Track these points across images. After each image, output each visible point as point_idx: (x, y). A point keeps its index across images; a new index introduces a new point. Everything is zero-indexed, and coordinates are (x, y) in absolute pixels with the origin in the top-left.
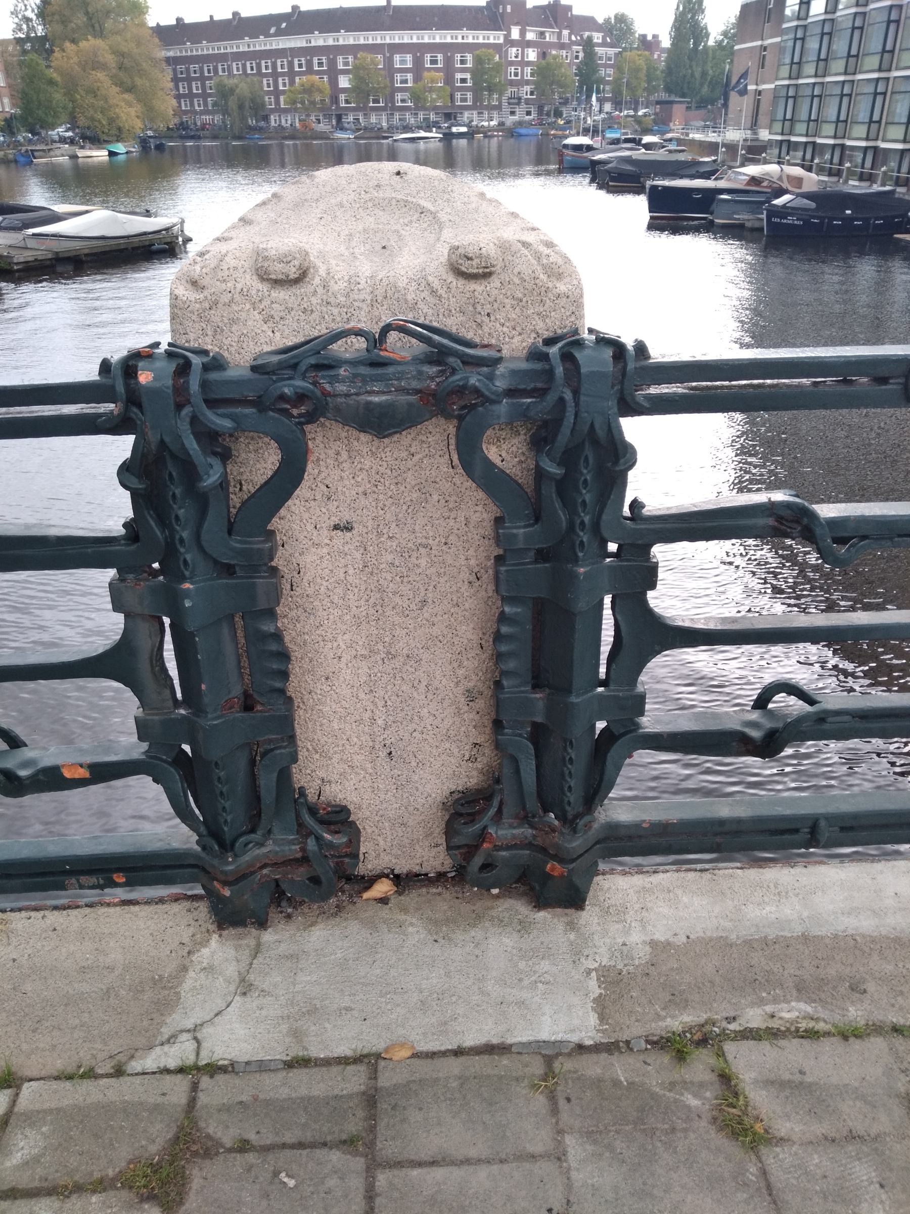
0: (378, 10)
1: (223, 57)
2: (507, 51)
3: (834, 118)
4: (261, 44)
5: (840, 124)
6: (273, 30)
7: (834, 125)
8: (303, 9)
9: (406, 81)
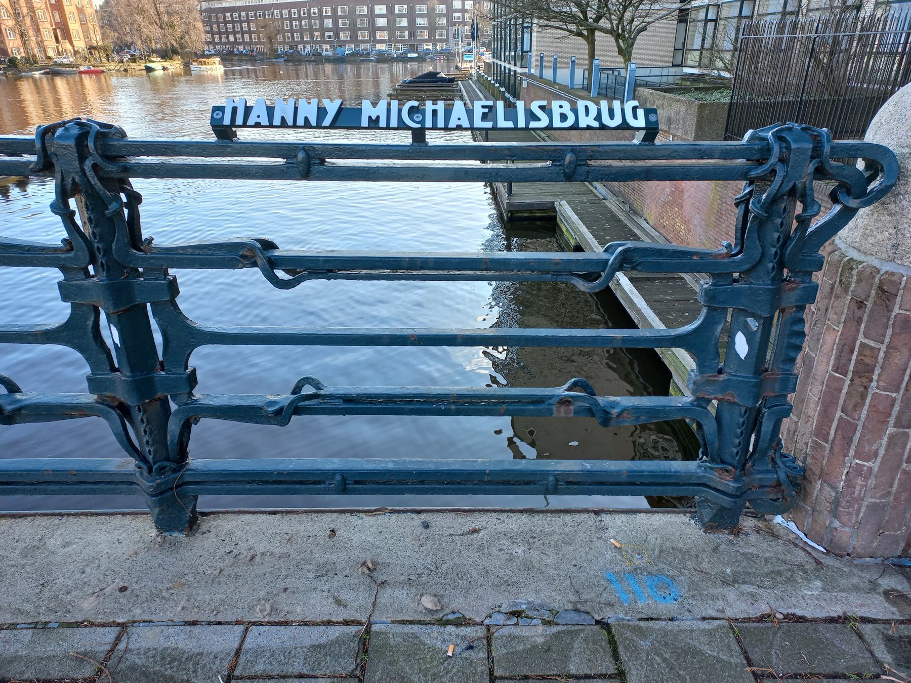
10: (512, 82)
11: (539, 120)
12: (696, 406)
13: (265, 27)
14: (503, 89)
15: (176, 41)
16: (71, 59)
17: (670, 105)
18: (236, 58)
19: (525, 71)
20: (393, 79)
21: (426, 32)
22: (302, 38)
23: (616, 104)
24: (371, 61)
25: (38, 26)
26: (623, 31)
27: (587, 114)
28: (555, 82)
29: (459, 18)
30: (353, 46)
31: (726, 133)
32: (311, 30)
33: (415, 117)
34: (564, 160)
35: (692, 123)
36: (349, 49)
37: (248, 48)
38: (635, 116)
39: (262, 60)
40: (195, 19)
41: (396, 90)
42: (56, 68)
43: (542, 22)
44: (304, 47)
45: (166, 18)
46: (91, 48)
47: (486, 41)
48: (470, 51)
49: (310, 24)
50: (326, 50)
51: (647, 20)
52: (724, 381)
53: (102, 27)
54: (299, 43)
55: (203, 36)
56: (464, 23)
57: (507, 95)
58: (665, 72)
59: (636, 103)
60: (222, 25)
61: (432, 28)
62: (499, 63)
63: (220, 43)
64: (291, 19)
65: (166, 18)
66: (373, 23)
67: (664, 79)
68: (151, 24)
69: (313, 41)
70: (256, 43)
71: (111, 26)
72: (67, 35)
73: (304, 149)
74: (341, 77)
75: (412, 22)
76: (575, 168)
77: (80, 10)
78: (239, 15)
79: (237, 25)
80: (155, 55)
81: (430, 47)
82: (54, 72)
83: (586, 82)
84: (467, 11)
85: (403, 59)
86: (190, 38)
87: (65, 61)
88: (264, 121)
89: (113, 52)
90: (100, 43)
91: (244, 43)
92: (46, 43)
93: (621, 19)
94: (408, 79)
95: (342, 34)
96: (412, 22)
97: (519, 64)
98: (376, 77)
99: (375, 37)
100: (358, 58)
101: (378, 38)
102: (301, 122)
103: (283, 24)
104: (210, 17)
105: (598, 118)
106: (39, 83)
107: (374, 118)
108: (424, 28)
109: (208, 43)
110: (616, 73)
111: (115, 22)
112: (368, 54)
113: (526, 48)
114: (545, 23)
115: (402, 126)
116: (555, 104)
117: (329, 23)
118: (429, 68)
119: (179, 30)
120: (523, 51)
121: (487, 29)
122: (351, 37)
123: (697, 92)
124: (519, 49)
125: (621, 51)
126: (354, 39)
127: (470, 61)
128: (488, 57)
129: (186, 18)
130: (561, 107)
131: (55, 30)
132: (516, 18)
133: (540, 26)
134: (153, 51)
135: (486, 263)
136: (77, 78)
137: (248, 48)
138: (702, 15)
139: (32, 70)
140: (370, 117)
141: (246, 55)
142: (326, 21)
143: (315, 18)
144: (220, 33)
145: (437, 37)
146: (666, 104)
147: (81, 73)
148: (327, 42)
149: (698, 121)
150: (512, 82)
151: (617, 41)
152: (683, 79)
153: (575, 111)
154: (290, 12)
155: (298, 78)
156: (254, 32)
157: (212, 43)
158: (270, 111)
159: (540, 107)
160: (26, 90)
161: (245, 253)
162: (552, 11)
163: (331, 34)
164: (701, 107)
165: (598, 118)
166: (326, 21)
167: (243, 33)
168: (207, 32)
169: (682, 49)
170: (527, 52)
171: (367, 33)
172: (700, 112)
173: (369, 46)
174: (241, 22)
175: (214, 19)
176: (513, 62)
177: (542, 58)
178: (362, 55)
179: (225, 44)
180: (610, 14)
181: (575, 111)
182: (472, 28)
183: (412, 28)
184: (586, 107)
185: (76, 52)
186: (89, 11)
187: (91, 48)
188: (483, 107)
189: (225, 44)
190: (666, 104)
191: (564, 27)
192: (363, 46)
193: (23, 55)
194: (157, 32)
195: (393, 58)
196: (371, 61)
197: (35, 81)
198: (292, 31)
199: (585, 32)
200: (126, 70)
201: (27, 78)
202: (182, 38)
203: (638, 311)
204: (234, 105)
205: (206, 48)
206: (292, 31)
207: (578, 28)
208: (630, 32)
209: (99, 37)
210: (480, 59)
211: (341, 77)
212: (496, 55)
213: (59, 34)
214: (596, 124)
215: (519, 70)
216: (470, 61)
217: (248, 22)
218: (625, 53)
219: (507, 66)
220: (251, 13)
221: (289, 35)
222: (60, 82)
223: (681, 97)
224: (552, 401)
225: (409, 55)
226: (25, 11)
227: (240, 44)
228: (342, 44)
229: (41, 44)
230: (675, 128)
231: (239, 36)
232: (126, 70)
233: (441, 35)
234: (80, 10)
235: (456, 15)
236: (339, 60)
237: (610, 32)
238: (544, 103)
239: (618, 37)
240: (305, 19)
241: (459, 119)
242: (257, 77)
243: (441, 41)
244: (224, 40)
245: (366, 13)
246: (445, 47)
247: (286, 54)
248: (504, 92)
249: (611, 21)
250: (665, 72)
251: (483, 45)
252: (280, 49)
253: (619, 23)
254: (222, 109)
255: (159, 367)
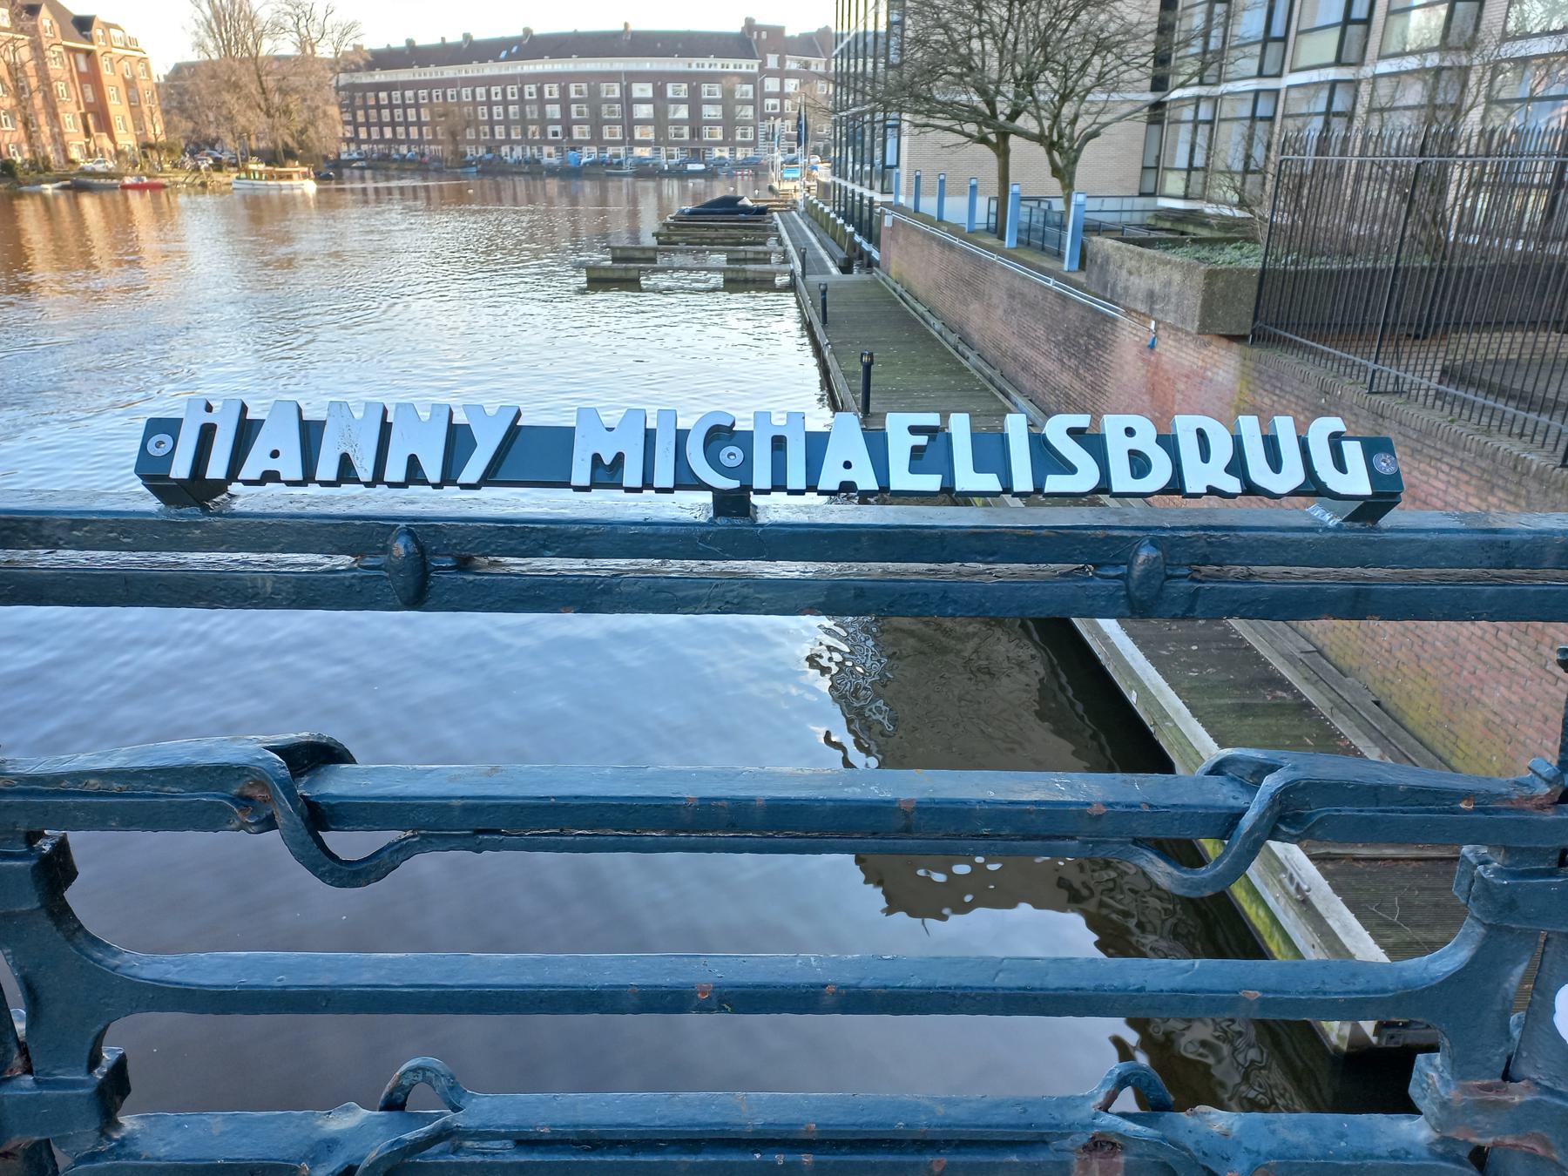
0: (615, 36)
1: (451, 83)
2: (762, 82)
3: (1185, 165)
4: (490, 69)
5: (1250, 177)
6: (503, 54)
7: (1184, 175)
8: (536, 32)
9: (613, 112)
10: (866, 215)
11: (1070, 469)
12: (1443, 1157)
13: (445, 115)
14: (850, 229)
15: (292, 136)
16: (110, 165)
17: (1153, 270)
18: (394, 166)
19: (889, 198)
20: (662, 209)
21: (719, 130)
22: (508, 134)
23: (1285, 428)
24: (625, 175)
25: (54, 108)
26: (1061, 136)
27: (1205, 455)
28: (940, 220)
29: (774, 107)
30: (594, 149)
31: (1255, 319)
32: (524, 122)
33: (723, 456)
34: (1130, 564)
35: (1194, 301)
36: (588, 155)
37: (415, 149)
38: (1340, 465)
39: (438, 171)
40: (327, 102)
41: (667, 225)
42: (82, 179)
43: (920, 119)
44: (512, 150)
45: (276, 99)
46: (146, 147)
47: (821, 145)
48: (793, 162)
49: (522, 112)
50: (550, 155)
51: (1103, 119)
52: (1521, 1105)
53: (166, 112)
54: (503, 143)
55: (339, 129)
56: (782, 116)
57: (858, 238)
58: (1127, 204)
59: (1336, 424)
60: (373, 113)
61: (729, 122)
62: (844, 183)
63: (368, 141)
64: (490, 104)
65: (276, 99)
66: (630, 112)
67: (1126, 217)
68: (250, 107)
69: (526, 141)
70: (430, 143)
71: (182, 110)
72: (105, 124)
73: (409, 532)
74: (574, 201)
75: (695, 112)
76: (1162, 589)
77: (130, 84)
78: (403, 96)
79: (398, 112)
80: (255, 159)
81: (726, 154)
82: (79, 185)
83: (993, 219)
84: (788, 96)
85: (680, 173)
86: (317, 132)
87: (99, 168)
88: (291, 467)
89: (183, 152)
90: (162, 138)
91: (409, 141)
92: (66, 138)
93: (1056, 117)
94: (688, 207)
95: (576, 129)
96: (695, 112)
97: (877, 185)
98: (634, 201)
99: (632, 135)
100: (602, 171)
101: (637, 136)
102: (395, 470)
103: (475, 111)
104: (352, 98)
105: (1237, 466)
106: (52, 203)
107: (607, 460)
108: (716, 123)
109: (349, 141)
110: (1044, 206)
111: (189, 105)
112: (620, 163)
113: (890, 161)
114: (925, 120)
115: (686, 481)
116: (1113, 426)
117: (554, 111)
118: (720, 190)
119: (298, 121)
120: (885, 167)
121: (823, 128)
122: (592, 133)
123: (1197, 247)
124: (877, 161)
125: (1056, 171)
126: (597, 139)
127: (794, 180)
128: (824, 173)
129: (312, 99)
130: (1130, 432)
131: (84, 117)
132: (873, 112)
133: (917, 126)
134: (253, 153)
135: (906, 814)
136: (118, 194)
137: (415, 149)
138: (1188, 113)
139: (41, 182)
140: (596, 459)
141: (411, 161)
142: (548, 108)
143: (530, 102)
144: (368, 125)
145: (738, 138)
146: (1144, 268)
147: (125, 187)
148: (550, 143)
149: (1204, 300)
150: (866, 215)
151: (1049, 153)
152: (1158, 218)
153: (1168, 442)
154: (488, 93)
155: (500, 200)
156: (426, 124)
157: (355, 140)
158: (310, 434)
159: (1074, 433)
160: (29, 215)
161: (249, 792)
162: (938, 102)
163: (558, 128)
164: (1211, 275)
165: (1237, 466)
166: (548, 108)
167: (407, 124)
168: (346, 123)
169: (1154, 168)
170: (891, 167)
171: (618, 129)
172: (1208, 285)
173: (622, 150)
174: (405, 107)
175: (358, 102)
176: (867, 183)
177: (918, 178)
178: (610, 165)
179: (376, 142)
180: (1038, 108)
181: (1168, 442)
182: (799, 126)
183: (696, 123)
184: (1201, 434)
185: (119, 154)
186: (144, 86)
187: (146, 147)
188: (914, 430)
189: (376, 142)
190: (1144, 268)
191: (958, 128)
192: (611, 151)
193: (27, 156)
194: (260, 122)
195: (662, 171)
196: (625, 175)
197: (45, 199)
198: (491, 123)
199: (993, 138)
200: (203, 185)
201: (31, 195)
202: (303, 131)
203: (1143, 689)
204: (209, 418)
205: (344, 148)
206: (491, 123)
207: (980, 131)
208: (1071, 139)
209: (159, 128)
210: (809, 176)
211: (574, 201)
212: (838, 169)
213: (91, 122)
214: (1233, 485)
215: (878, 198)
216: (794, 180)
217: (417, 106)
218: (1064, 174)
219: (858, 190)
220: (423, 93)
221: (487, 129)
222: (88, 203)
223: (1168, 256)
224: (1067, 1143)
225: (690, 167)
226: (34, 82)
227: (401, 142)
228: (576, 146)
229: (58, 138)
230: (1162, 311)
231: (400, 130)
232: (203, 185)
233: (744, 135)
234: (130, 84)
235: (770, 102)
236: (570, 173)
237: (1039, 138)
238: (1082, 421)
239: (1051, 146)
240: (513, 103)
241: (847, 465)
242: (429, 199)
243: (744, 144)
244: (375, 136)
245: (617, 95)
246: (751, 154)
247: (480, 160)
248: (852, 234)
249: (1039, 119)
250: (1127, 204)
251: (816, 151)
252: (471, 152)
253: (1054, 123)
254: (170, 427)
255: (17, 1061)
